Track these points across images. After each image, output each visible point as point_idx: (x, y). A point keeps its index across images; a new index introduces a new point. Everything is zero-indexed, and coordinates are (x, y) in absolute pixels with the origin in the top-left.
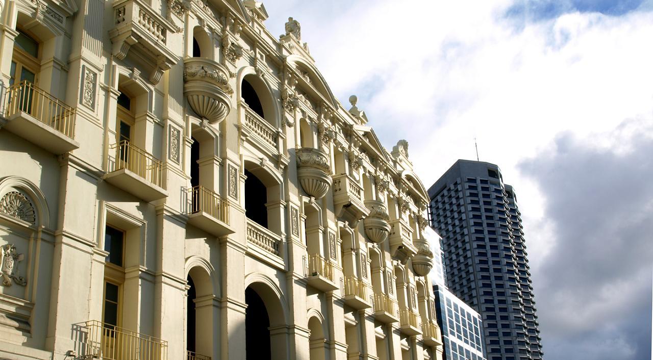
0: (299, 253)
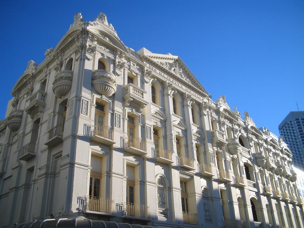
0: (261, 186)
